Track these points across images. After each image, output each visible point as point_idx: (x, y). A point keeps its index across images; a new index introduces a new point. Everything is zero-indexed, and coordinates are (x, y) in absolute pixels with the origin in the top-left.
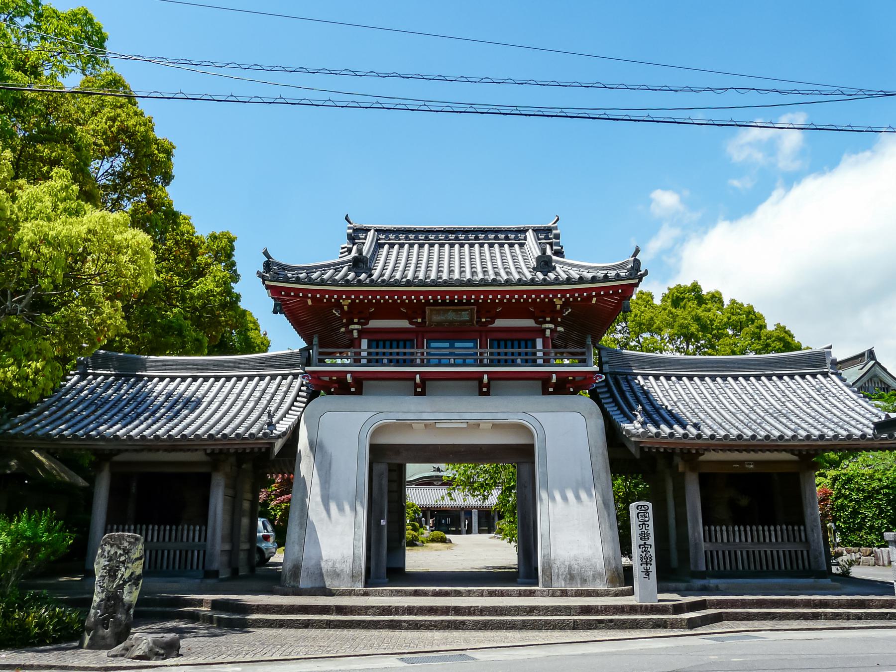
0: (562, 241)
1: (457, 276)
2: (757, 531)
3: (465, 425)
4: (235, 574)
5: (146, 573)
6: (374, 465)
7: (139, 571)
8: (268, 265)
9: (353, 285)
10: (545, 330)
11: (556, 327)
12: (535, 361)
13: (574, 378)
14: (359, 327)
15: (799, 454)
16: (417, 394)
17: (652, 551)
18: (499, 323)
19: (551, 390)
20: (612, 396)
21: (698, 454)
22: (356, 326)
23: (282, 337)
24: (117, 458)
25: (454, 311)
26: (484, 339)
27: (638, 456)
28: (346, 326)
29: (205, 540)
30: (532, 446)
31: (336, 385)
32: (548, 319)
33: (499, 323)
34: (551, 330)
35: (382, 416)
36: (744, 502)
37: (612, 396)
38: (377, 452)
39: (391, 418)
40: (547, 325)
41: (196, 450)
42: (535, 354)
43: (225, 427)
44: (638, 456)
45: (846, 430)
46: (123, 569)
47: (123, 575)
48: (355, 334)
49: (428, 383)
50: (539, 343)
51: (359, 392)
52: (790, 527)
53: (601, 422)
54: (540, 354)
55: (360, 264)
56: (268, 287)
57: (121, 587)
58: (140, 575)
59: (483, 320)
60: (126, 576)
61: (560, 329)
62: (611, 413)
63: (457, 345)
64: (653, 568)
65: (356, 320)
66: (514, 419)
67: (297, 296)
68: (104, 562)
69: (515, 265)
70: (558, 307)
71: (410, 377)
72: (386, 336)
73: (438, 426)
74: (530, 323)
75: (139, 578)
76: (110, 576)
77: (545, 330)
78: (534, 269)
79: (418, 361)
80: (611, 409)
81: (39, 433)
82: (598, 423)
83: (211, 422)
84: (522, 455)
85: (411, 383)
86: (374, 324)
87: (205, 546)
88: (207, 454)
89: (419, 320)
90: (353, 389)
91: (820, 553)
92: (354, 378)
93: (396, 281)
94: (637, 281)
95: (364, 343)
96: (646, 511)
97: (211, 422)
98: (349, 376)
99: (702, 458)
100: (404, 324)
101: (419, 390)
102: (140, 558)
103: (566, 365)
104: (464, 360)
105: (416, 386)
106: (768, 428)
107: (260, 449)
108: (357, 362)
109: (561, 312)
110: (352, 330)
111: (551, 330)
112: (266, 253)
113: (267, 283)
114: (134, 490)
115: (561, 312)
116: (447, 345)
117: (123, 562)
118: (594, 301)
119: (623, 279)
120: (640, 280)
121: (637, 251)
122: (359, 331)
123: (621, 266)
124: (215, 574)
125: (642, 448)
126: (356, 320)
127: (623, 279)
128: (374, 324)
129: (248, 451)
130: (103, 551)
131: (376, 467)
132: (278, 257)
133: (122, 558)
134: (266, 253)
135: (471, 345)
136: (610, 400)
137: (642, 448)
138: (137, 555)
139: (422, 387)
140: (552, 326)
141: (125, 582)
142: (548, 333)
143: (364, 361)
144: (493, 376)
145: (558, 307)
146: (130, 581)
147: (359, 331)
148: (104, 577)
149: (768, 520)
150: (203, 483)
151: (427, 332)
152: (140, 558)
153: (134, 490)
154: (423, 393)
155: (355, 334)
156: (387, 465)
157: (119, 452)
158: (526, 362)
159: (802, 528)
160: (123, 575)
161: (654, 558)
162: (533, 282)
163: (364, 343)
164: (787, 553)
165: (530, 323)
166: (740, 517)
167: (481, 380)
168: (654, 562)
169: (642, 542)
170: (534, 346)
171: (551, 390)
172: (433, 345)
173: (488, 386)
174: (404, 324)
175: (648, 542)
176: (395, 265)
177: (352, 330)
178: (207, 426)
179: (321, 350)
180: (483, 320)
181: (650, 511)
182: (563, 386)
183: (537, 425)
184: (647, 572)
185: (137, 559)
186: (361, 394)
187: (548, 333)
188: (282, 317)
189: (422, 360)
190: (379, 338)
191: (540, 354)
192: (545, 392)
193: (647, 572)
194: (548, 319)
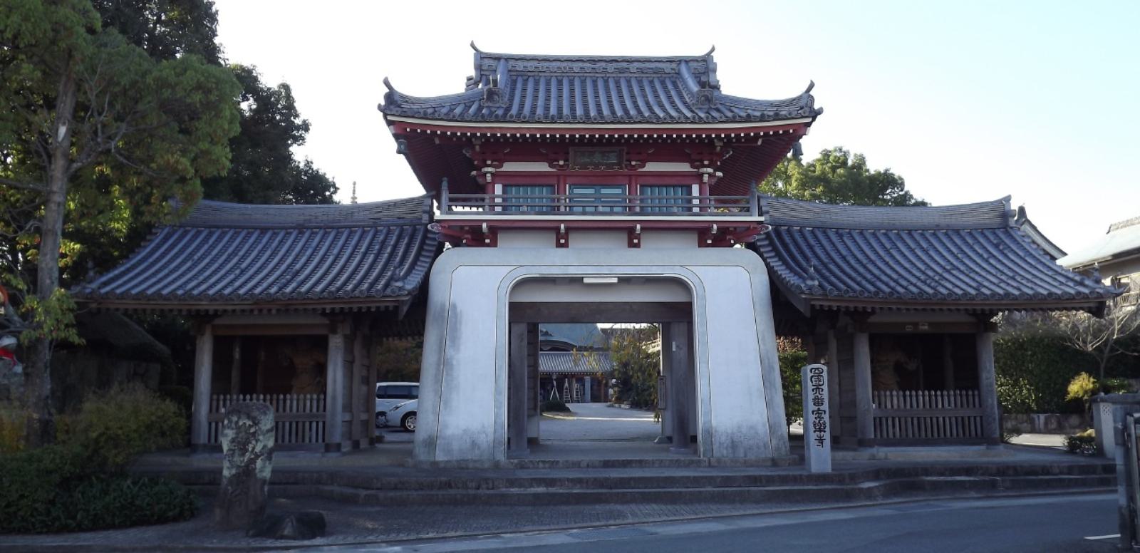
2: (930, 396)
3: (615, 280)
4: (356, 445)
5: (277, 447)
6: (512, 324)
7: (271, 444)
10: (702, 174)
11: (715, 171)
12: (690, 209)
17: (826, 418)
19: (709, 242)
22: (490, 169)
24: (218, 321)
26: (633, 184)
27: (808, 314)
28: (478, 168)
29: (324, 410)
31: (469, 236)
34: (710, 175)
36: (912, 366)
37: (775, 249)
38: (517, 312)
40: (705, 170)
43: (345, 283)
44: (808, 314)
46: (254, 442)
47: (254, 448)
48: (489, 178)
50: (695, 189)
52: (964, 392)
53: (765, 278)
54: (696, 202)
56: (390, 123)
58: (272, 448)
59: (633, 163)
60: (258, 449)
61: (719, 174)
62: (776, 268)
63: (604, 191)
64: (827, 436)
65: (489, 162)
68: (230, 433)
72: (674, 181)
73: (586, 281)
77: (702, 174)
79: (638, 209)
80: (776, 264)
81: (242, 291)
82: (762, 278)
87: (324, 416)
89: (561, 163)
91: (994, 419)
95: (498, 189)
96: (820, 374)
101: (563, 241)
103: (716, 217)
106: (950, 286)
107: (387, 307)
109: (721, 155)
111: (710, 175)
112: (387, 83)
113: (389, 118)
114: (237, 355)
116: (591, 191)
117: (254, 434)
120: (814, 119)
122: (493, 175)
124: (338, 447)
128: (509, 167)
129: (363, 310)
130: (230, 421)
131: (515, 328)
132: (406, 88)
133: (252, 430)
134: (387, 83)
135: (618, 191)
136: (773, 254)
137: (813, 306)
138: (269, 426)
140: (710, 170)
141: (257, 456)
143: (696, 210)
146: (262, 454)
147: (493, 175)
148: (234, 450)
149: (935, 382)
150: (320, 344)
151: (569, 176)
152: (271, 430)
153: (237, 355)
155: (489, 178)
156: (528, 322)
159: (976, 393)
160: (254, 448)
161: (828, 425)
163: (498, 189)
164: (960, 419)
165: (685, 167)
166: (907, 382)
168: (828, 429)
169: (816, 408)
170: (690, 193)
171: (709, 242)
172: (576, 191)
173: (638, 237)
174: (543, 167)
175: (822, 408)
177: (485, 174)
179: (452, 195)
180: (633, 163)
181: (825, 374)
182: (721, 237)
184: (821, 440)
185: (268, 431)
186: (495, 245)
187: (706, 178)
188: (402, 157)
189: (642, 208)
190: (511, 181)
191: (696, 202)
192: (702, 244)
193: (821, 440)
194: (706, 162)
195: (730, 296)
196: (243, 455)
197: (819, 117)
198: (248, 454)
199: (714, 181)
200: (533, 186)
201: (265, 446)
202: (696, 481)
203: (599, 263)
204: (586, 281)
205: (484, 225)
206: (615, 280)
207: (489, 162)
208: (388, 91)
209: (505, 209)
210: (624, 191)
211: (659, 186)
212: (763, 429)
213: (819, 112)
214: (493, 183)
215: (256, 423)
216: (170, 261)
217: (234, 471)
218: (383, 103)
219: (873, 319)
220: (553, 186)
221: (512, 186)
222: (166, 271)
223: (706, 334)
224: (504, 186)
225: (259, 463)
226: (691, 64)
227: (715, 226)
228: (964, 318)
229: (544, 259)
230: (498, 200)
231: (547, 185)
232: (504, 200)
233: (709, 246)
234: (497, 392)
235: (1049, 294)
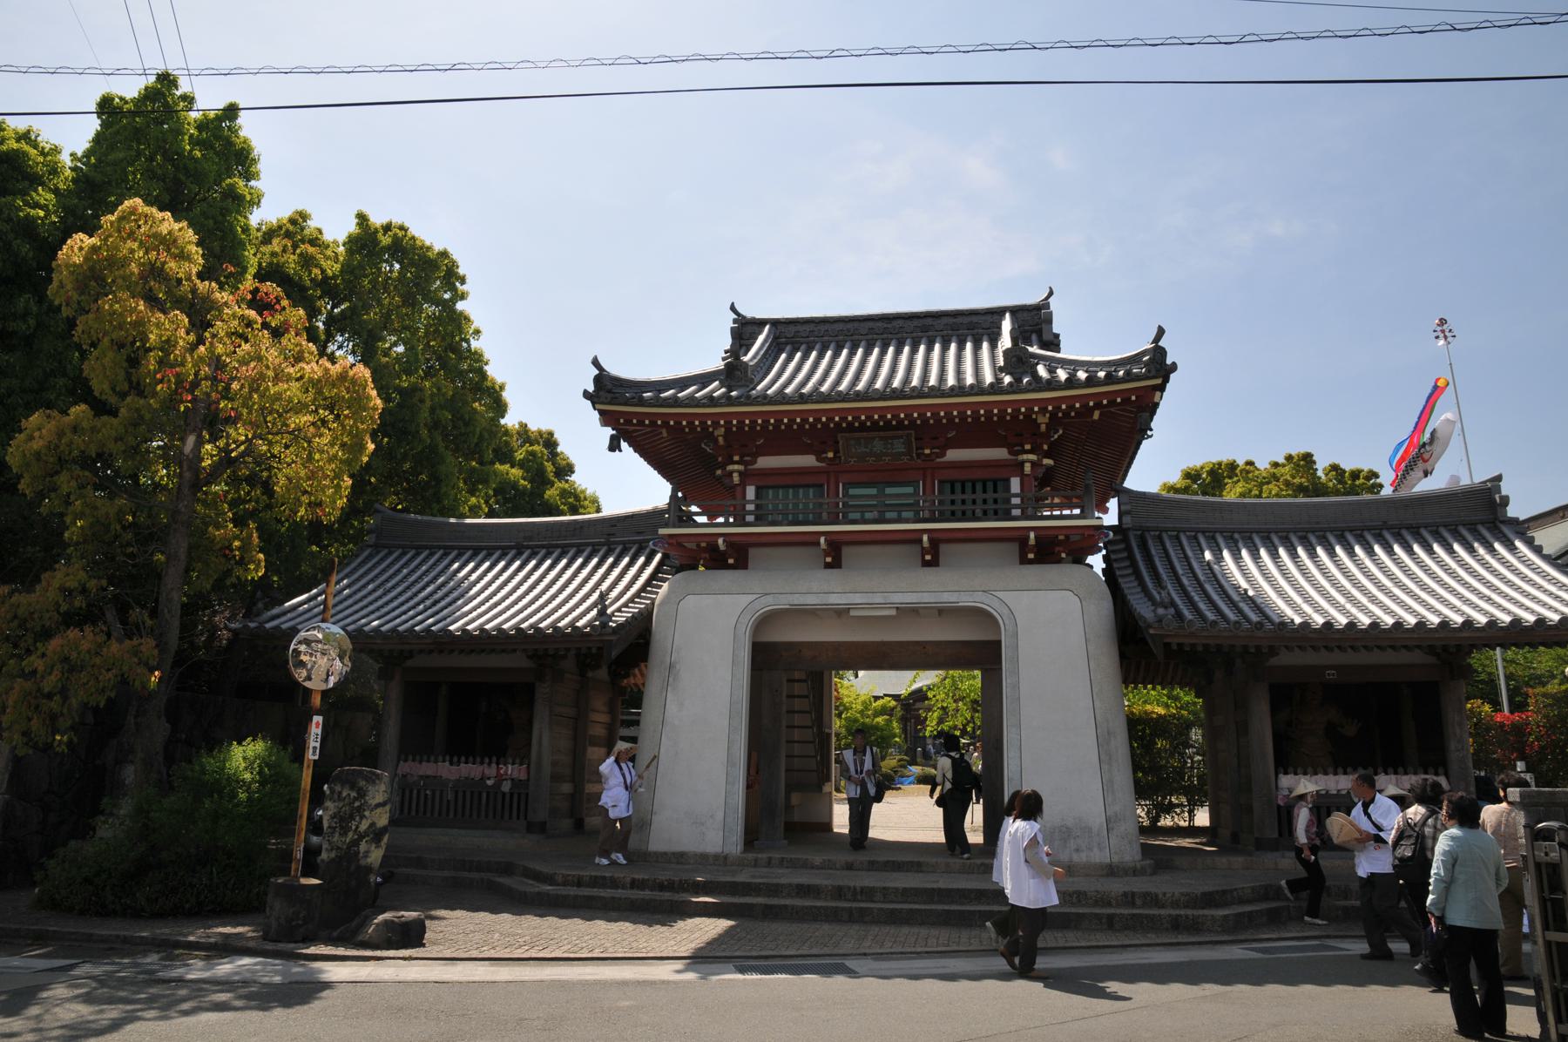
0: (1435, 327)
1: (933, 381)
3: (893, 612)
8: (598, 380)
9: (721, 405)
10: (1022, 463)
13: (1067, 537)
14: (741, 467)
15: (534, 656)
16: (926, 564)
18: (953, 455)
20: (1134, 565)
21: (1273, 651)
22: (736, 467)
23: (625, 484)
24: (409, 663)
25: (881, 438)
28: (723, 467)
30: (999, 642)
32: (1028, 447)
33: (953, 455)
34: (1033, 463)
35: (769, 599)
36: (1350, 730)
39: (783, 602)
40: (1025, 457)
41: (514, 651)
42: (1008, 501)
45: (1486, 613)
49: (943, 548)
50: (1015, 485)
51: (742, 564)
55: (734, 372)
57: (356, 843)
59: (927, 451)
60: (364, 826)
61: (1047, 461)
63: (888, 491)
66: (966, 600)
67: (641, 423)
69: (978, 366)
70: (1043, 427)
71: (810, 541)
73: (853, 613)
74: (1000, 453)
75: (384, 830)
76: (342, 828)
77: (1022, 463)
78: (1001, 369)
83: (561, 612)
84: (984, 655)
85: (916, 549)
86: (765, 462)
88: (529, 657)
89: (830, 455)
90: (731, 561)
92: (830, 543)
93: (858, 393)
94: (1159, 381)
95: (751, 492)
97: (561, 612)
98: (720, 541)
99: (1274, 661)
100: (808, 461)
101: (928, 557)
102: (383, 805)
104: (882, 513)
105: (924, 552)
108: (741, 522)
109: (1047, 435)
110: (731, 473)
111: (1033, 463)
112: (596, 363)
115: (1047, 435)
116: (873, 491)
118: (1096, 415)
119: (1138, 378)
121: (1161, 332)
122: (741, 473)
123: (1135, 359)
125: (1167, 645)
126: (736, 458)
127: (1138, 378)
128: (765, 462)
132: (629, 367)
133: (357, 804)
134: (596, 363)
135: (910, 490)
138: (380, 798)
139: (835, 555)
140: (1033, 457)
141: (361, 837)
142: (1028, 468)
144: (937, 540)
145: (1043, 427)
154: (934, 563)
157: (411, 655)
158: (997, 516)
162: (996, 387)
163: (751, 492)
165: (1000, 453)
167: (1023, 541)
170: (1008, 488)
171: (1031, 556)
172: (852, 491)
174: (808, 461)
176: (793, 376)
177: (731, 473)
178: (570, 618)
183: (1005, 611)
187: (1028, 468)
190: (767, 481)
192: (1024, 561)
194: (1028, 447)
195: (1054, 628)
196: (345, 834)
197: (1172, 376)
198: (350, 834)
199: (1040, 472)
200: (796, 487)
201: (373, 824)
202: (804, 890)
203: (877, 591)
204: (893, 612)
205: (720, 541)
206: (853, 613)
207: (736, 458)
208: (597, 372)
209: (760, 520)
210: (916, 492)
211: (793, 487)
212: (1096, 818)
213: (1174, 367)
214: (743, 484)
215: (362, 794)
216: (494, 594)
217: (333, 855)
218: (591, 389)
219: (1274, 661)
220: (821, 486)
221: (768, 487)
222: (1494, 596)
223: (1016, 686)
224: (758, 489)
225: (363, 846)
226: (1020, 315)
227: (1032, 535)
228: (1417, 657)
229: (815, 588)
230: (750, 507)
231: (813, 486)
232: (757, 507)
233: (1031, 562)
234: (730, 762)
235: (1537, 622)
